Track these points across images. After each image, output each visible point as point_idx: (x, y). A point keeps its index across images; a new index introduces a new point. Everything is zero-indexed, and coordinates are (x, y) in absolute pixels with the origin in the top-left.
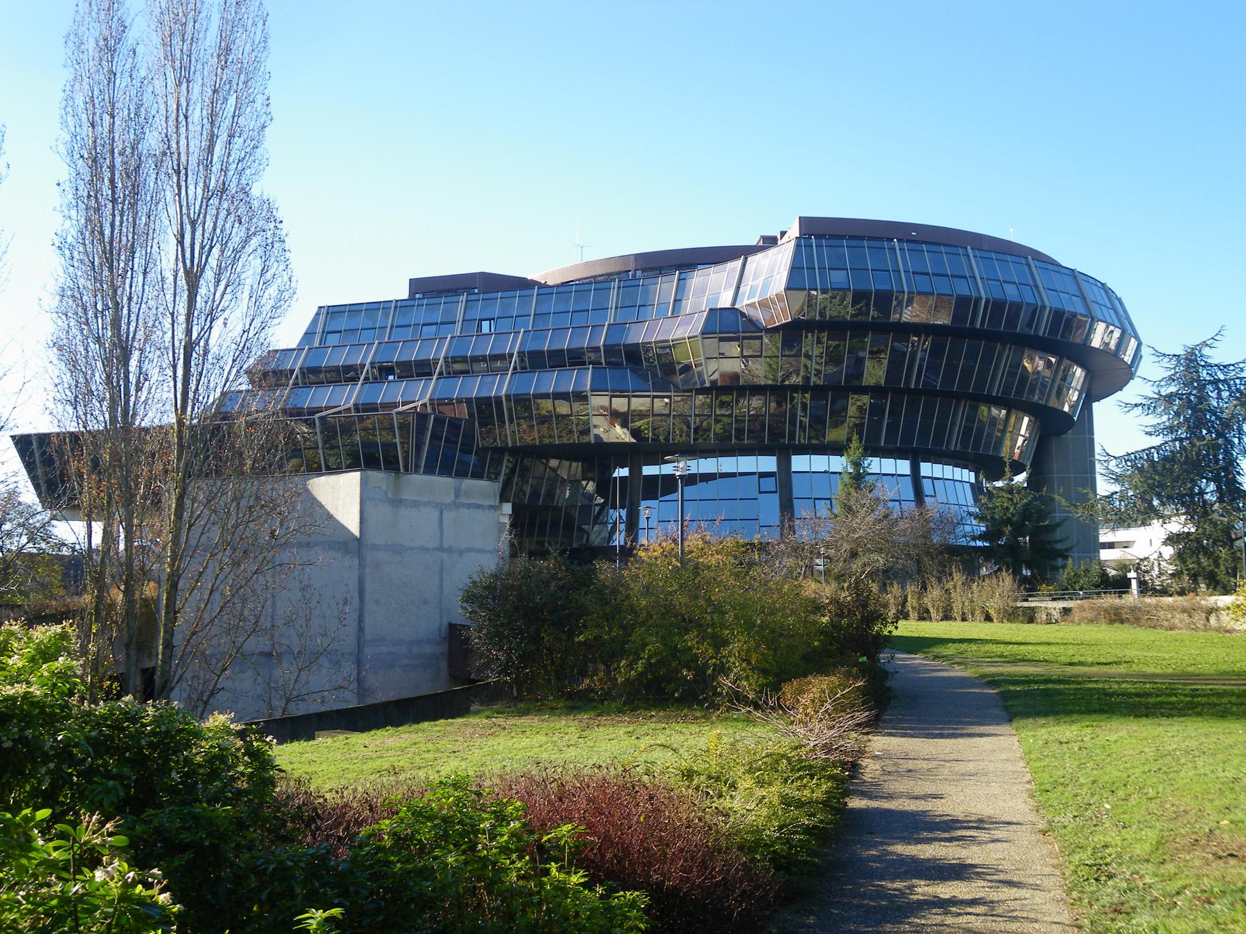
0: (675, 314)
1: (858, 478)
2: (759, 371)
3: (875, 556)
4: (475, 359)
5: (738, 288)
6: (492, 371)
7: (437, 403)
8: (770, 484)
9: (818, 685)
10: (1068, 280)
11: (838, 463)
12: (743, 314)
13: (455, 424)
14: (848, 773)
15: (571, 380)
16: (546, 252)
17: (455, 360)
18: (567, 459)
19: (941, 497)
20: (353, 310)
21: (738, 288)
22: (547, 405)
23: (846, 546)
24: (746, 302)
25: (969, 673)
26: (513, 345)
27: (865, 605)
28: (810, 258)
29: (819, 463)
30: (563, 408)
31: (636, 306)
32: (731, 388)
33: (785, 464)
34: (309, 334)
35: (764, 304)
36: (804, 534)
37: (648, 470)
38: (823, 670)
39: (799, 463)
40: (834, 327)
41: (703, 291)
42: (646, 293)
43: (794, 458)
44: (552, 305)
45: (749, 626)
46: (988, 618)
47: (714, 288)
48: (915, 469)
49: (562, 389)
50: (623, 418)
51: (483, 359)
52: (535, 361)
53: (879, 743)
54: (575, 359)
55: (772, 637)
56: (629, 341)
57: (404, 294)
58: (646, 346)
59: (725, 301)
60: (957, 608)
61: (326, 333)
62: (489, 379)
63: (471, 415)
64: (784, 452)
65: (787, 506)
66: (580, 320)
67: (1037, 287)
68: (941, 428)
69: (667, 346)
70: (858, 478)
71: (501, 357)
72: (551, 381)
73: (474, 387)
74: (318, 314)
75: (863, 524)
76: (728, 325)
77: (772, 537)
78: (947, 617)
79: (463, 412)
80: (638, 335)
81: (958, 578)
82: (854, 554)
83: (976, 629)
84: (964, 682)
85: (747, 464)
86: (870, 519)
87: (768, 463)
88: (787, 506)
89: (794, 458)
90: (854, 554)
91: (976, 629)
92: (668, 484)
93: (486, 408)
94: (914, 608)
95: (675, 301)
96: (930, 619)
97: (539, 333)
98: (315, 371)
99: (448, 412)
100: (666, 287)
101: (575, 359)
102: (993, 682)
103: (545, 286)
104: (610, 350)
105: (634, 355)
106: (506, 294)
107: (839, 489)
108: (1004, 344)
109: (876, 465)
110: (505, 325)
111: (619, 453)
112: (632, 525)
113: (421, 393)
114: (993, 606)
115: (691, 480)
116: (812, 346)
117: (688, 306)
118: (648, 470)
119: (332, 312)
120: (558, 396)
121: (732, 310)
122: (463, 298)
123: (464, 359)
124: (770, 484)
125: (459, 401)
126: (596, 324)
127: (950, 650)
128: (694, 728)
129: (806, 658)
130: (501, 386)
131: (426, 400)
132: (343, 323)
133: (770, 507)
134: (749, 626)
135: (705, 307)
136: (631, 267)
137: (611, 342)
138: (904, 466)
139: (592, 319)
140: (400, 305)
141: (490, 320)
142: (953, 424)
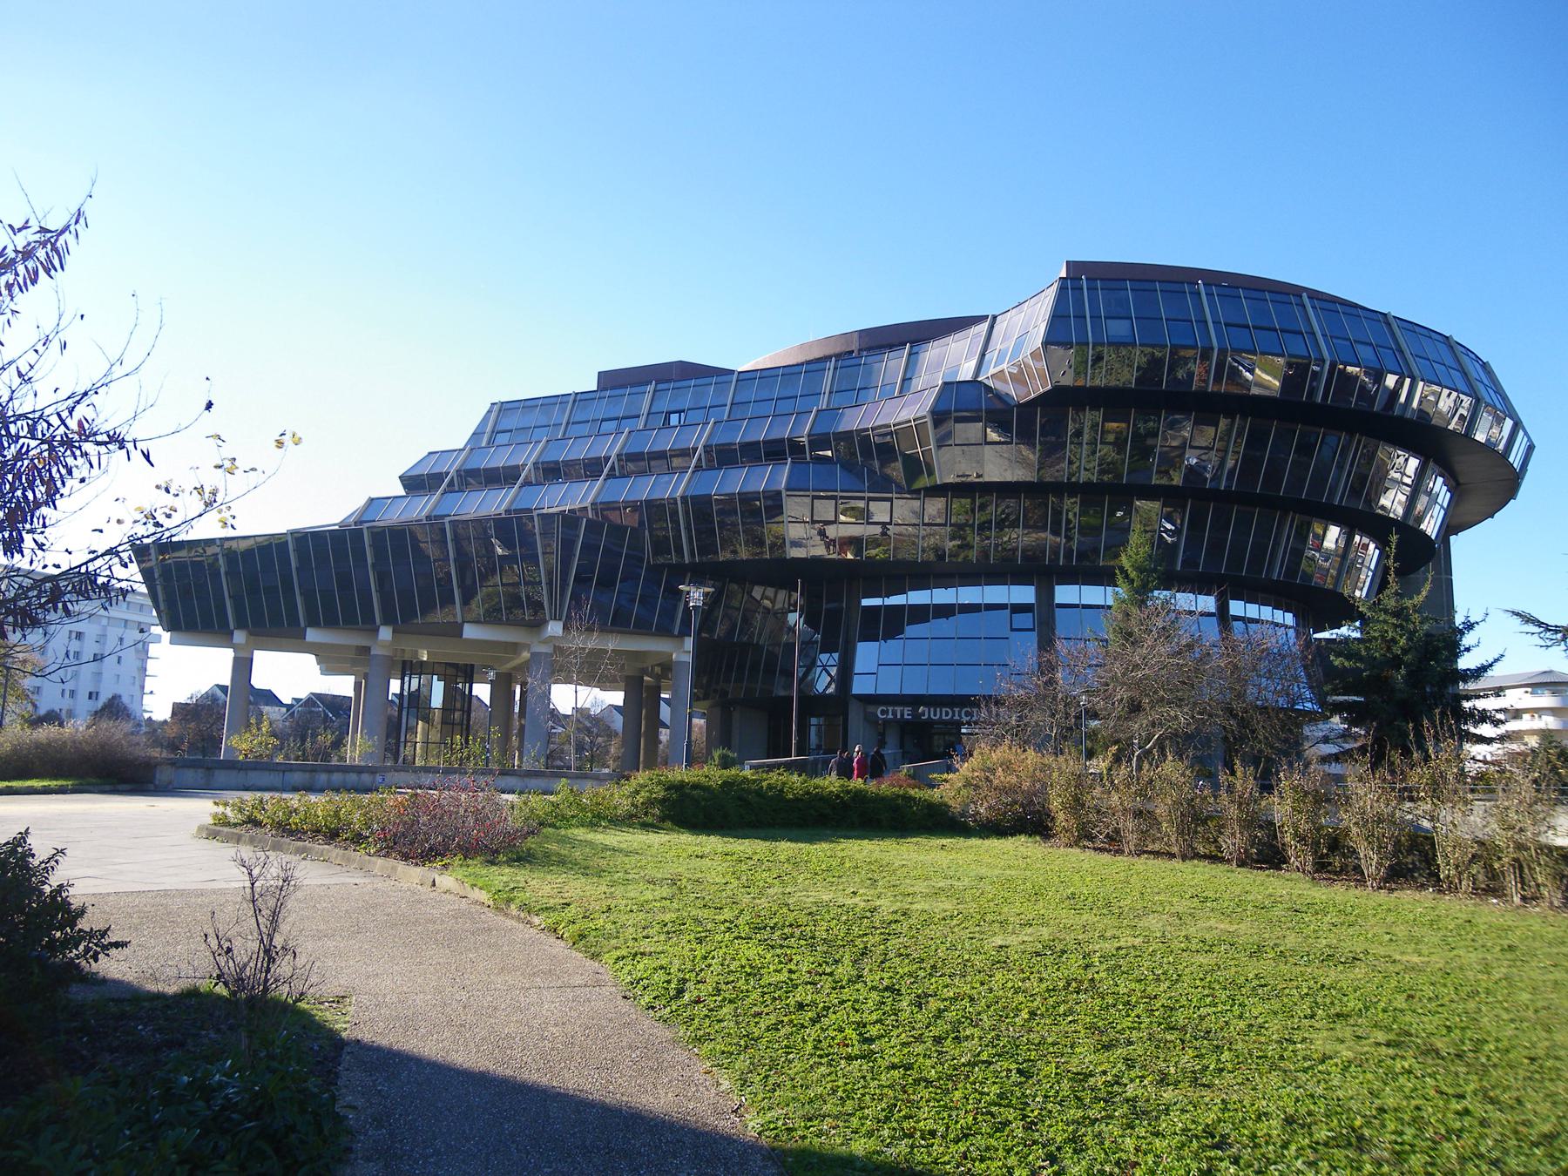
5: (983, 355)
6: (671, 471)
7: (603, 508)
8: (1025, 620)
10: (1442, 348)
12: (988, 388)
13: (618, 531)
16: (752, 331)
18: (772, 586)
20: (528, 405)
21: (983, 355)
23: (1122, 694)
24: (992, 371)
26: (698, 439)
28: (1079, 303)
29: (1093, 594)
33: (1046, 595)
34: (476, 434)
35: (1018, 379)
40: (1111, 401)
41: (940, 365)
43: (1057, 588)
44: (752, 393)
47: (954, 359)
48: (1223, 609)
52: (723, 456)
54: (774, 451)
56: (841, 429)
57: (592, 385)
59: (966, 372)
61: (495, 432)
62: (666, 478)
63: (641, 523)
67: (1401, 352)
68: (1259, 550)
69: (884, 430)
72: (737, 481)
73: (644, 488)
74: (489, 412)
76: (965, 404)
79: (629, 520)
82: (1135, 708)
87: (1024, 594)
89: (1057, 588)
90: (1135, 708)
94: (1301, 839)
95: (904, 380)
96: (1361, 882)
98: (473, 473)
99: (614, 516)
100: (894, 364)
106: (699, 381)
108: (1351, 434)
113: (578, 496)
117: (918, 383)
119: (503, 409)
121: (974, 382)
122: (651, 388)
125: (627, 504)
126: (812, 422)
131: (587, 504)
132: (512, 422)
136: (855, 347)
137: (817, 430)
138: (1208, 603)
139: (800, 404)
140: (580, 399)
141: (679, 412)
142: (1277, 543)
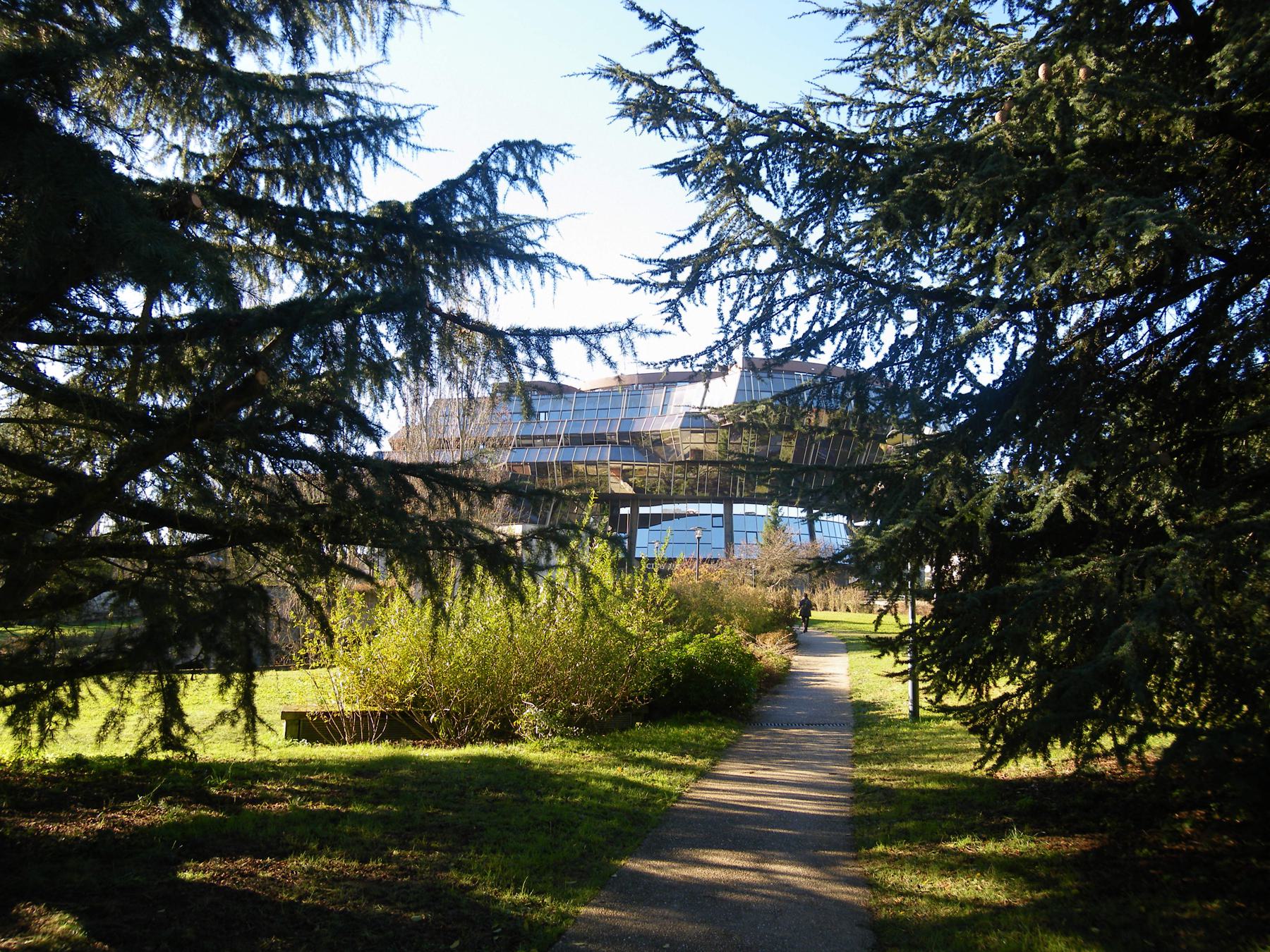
0: (663, 413)
1: (776, 521)
2: (712, 450)
3: (785, 571)
4: (535, 438)
8: (718, 521)
9: (771, 636)
11: (762, 510)
14: (789, 662)
15: (596, 453)
17: (523, 437)
19: (825, 532)
22: (581, 467)
25: (834, 636)
27: (789, 603)
30: (592, 470)
31: (638, 407)
32: (697, 458)
33: (729, 510)
36: (739, 554)
37: (643, 510)
38: (773, 630)
39: (738, 509)
42: (645, 399)
44: (585, 405)
45: (742, 612)
46: (848, 610)
49: (591, 459)
50: (625, 476)
51: (540, 437)
52: (576, 440)
53: (796, 658)
54: (600, 440)
55: (751, 616)
58: (645, 435)
60: (831, 607)
64: (729, 502)
65: (729, 538)
66: (603, 415)
70: (776, 521)
71: (552, 437)
72: (584, 453)
73: (535, 455)
75: (779, 552)
77: (720, 555)
78: (825, 609)
80: (640, 426)
81: (833, 586)
82: (772, 569)
83: (841, 615)
84: (831, 639)
85: (705, 508)
86: (783, 548)
87: (718, 508)
88: (729, 538)
90: (772, 569)
91: (841, 615)
92: (656, 519)
93: (542, 469)
97: (577, 422)
100: (658, 396)
101: (600, 440)
102: (843, 640)
103: (580, 392)
104: (622, 435)
105: (637, 436)
107: (763, 528)
109: (786, 511)
110: (555, 416)
111: (624, 499)
112: (1101, 746)
114: (851, 603)
115: (669, 517)
116: (748, 437)
117: (671, 409)
118: (643, 510)
120: (588, 463)
123: (529, 437)
124: (718, 521)
127: (826, 625)
128: (356, 757)
129: (764, 627)
130: (553, 455)
133: (718, 537)
134: (742, 612)
135: (683, 411)
136: (636, 382)
